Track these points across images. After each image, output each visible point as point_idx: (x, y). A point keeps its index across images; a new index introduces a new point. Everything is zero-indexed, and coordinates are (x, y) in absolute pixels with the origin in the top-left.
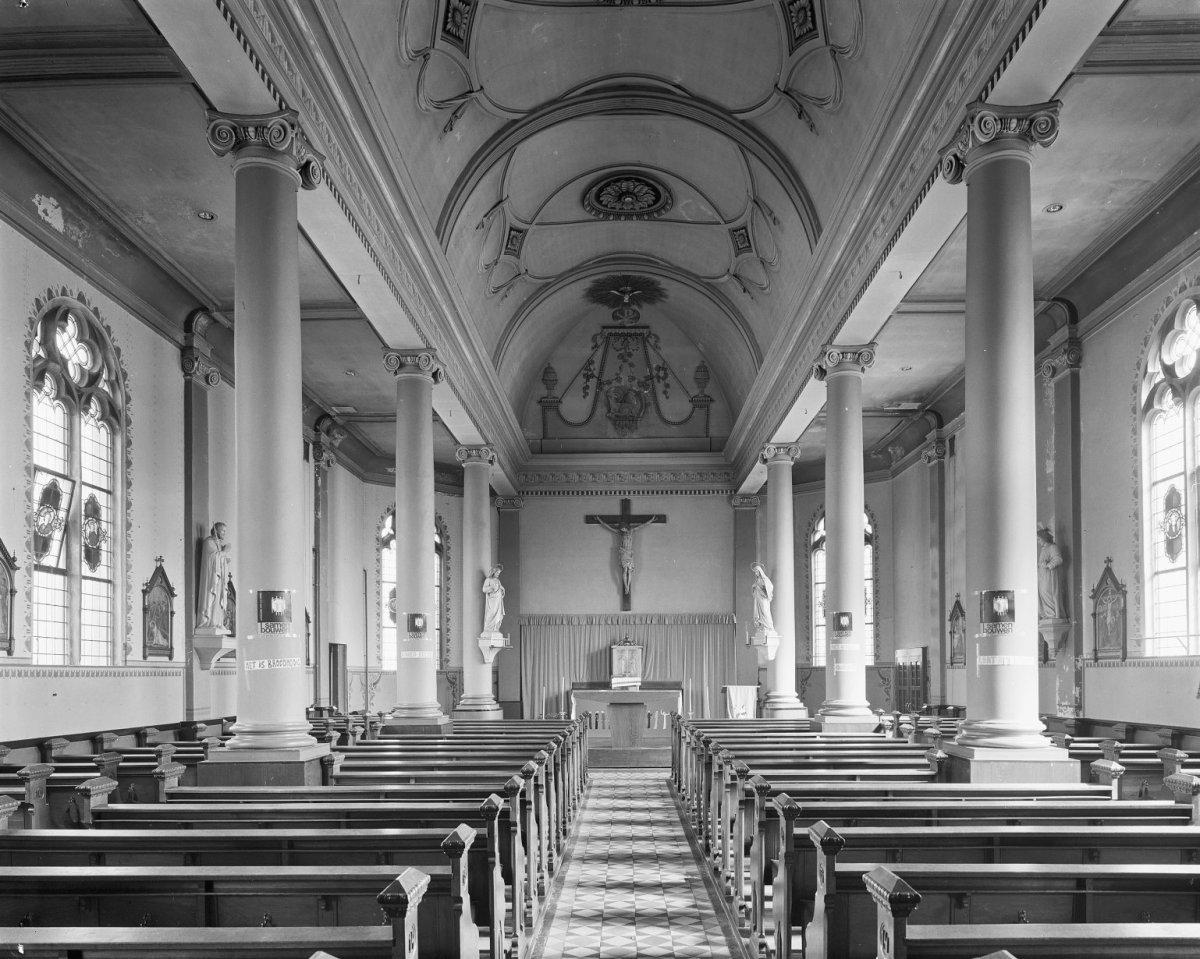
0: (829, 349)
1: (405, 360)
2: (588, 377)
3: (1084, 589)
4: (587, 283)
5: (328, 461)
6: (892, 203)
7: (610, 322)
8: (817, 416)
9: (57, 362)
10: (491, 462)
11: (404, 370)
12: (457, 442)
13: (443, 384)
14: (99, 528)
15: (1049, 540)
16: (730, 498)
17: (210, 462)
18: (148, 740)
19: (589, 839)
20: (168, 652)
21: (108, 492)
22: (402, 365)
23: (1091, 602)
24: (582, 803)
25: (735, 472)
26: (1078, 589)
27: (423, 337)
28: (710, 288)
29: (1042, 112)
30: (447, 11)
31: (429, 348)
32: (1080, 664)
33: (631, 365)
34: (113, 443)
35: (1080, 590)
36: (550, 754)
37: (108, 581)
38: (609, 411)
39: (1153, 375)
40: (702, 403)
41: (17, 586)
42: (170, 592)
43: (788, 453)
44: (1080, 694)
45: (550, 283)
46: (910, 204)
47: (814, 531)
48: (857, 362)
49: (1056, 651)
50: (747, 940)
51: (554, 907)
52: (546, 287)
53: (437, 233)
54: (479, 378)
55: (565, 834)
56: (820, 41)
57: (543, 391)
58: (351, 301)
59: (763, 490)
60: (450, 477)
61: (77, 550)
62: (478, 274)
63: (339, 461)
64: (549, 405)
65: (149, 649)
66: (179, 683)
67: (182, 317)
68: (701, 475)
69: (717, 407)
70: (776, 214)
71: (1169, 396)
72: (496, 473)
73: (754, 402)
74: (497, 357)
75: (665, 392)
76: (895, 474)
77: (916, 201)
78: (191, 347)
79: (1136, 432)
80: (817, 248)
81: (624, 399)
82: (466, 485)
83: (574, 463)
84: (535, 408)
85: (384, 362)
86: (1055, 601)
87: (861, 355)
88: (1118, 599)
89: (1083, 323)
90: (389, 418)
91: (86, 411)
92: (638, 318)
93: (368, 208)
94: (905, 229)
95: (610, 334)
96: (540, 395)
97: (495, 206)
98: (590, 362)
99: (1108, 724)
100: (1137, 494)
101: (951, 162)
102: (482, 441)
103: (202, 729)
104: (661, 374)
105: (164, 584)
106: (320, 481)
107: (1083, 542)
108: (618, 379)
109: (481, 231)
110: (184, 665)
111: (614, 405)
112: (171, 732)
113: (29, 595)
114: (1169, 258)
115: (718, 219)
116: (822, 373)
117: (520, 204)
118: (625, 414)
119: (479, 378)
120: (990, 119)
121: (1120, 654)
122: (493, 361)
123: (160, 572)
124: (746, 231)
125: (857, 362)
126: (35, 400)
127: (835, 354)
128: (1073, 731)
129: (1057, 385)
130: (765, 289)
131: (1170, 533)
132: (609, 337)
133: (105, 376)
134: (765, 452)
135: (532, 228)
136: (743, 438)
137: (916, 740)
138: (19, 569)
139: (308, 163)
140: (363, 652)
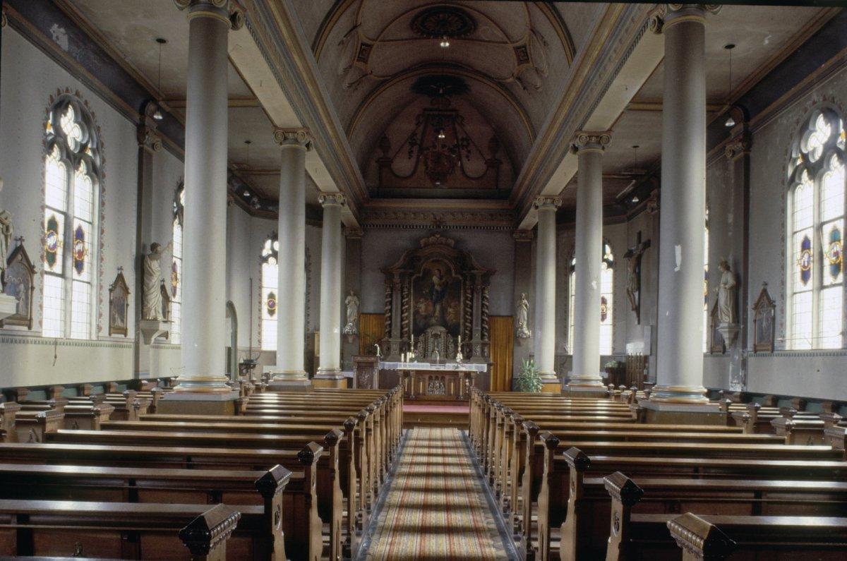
1: (285, 134)
2: (412, 145)
3: (749, 304)
6: (620, 40)
9: (61, 137)
10: (342, 204)
11: (287, 141)
12: (318, 189)
13: (313, 152)
14: (83, 247)
15: (727, 268)
16: (512, 233)
17: (153, 203)
18: (112, 390)
20: (27, 322)
21: (90, 223)
22: (285, 139)
23: (754, 312)
25: (517, 211)
26: (745, 303)
27: (302, 120)
32: (745, 355)
34: (93, 190)
35: (747, 304)
36: (371, 413)
37: (88, 283)
39: (795, 160)
40: (493, 164)
41: (35, 285)
42: (126, 290)
44: (745, 375)
45: (386, 80)
46: (643, 25)
48: (599, 143)
49: (730, 345)
50: (508, 520)
51: (384, 500)
53: (313, 48)
54: (336, 146)
55: (391, 460)
58: (252, 95)
59: (535, 228)
60: (314, 215)
61: (70, 262)
62: (338, 76)
64: (385, 164)
65: (114, 329)
66: (130, 353)
67: (138, 105)
68: (492, 215)
69: (506, 167)
70: (546, 38)
71: (805, 175)
72: (347, 213)
73: (529, 166)
74: (348, 131)
75: (467, 157)
76: (629, 218)
77: (633, 45)
78: (144, 125)
79: (784, 198)
83: (402, 205)
84: (374, 165)
86: (730, 309)
87: (599, 138)
88: (770, 311)
89: (752, 122)
90: (276, 172)
91: (77, 169)
97: (351, 30)
98: (414, 134)
99: (761, 395)
100: (784, 239)
101: (655, 20)
102: (298, 124)
103: (90, 389)
104: (465, 143)
105: (123, 286)
107: (750, 270)
109: (341, 46)
110: (133, 341)
112: (125, 385)
113: (41, 290)
114: (806, 81)
116: (575, 149)
118: (439, 170)
119: (336, 146)
121: (770, 348)
122: (346, 133)
123: (120, 278)
124: (526, 49)
126: (47, 161)
128: (798, 407)
129: (736, 162)
131: (804, 267)
133: (89, 146)
134: (537, 202)
135: (377, 43)
136: (522, 190)
138: (36, 273)
139: (236, 13)
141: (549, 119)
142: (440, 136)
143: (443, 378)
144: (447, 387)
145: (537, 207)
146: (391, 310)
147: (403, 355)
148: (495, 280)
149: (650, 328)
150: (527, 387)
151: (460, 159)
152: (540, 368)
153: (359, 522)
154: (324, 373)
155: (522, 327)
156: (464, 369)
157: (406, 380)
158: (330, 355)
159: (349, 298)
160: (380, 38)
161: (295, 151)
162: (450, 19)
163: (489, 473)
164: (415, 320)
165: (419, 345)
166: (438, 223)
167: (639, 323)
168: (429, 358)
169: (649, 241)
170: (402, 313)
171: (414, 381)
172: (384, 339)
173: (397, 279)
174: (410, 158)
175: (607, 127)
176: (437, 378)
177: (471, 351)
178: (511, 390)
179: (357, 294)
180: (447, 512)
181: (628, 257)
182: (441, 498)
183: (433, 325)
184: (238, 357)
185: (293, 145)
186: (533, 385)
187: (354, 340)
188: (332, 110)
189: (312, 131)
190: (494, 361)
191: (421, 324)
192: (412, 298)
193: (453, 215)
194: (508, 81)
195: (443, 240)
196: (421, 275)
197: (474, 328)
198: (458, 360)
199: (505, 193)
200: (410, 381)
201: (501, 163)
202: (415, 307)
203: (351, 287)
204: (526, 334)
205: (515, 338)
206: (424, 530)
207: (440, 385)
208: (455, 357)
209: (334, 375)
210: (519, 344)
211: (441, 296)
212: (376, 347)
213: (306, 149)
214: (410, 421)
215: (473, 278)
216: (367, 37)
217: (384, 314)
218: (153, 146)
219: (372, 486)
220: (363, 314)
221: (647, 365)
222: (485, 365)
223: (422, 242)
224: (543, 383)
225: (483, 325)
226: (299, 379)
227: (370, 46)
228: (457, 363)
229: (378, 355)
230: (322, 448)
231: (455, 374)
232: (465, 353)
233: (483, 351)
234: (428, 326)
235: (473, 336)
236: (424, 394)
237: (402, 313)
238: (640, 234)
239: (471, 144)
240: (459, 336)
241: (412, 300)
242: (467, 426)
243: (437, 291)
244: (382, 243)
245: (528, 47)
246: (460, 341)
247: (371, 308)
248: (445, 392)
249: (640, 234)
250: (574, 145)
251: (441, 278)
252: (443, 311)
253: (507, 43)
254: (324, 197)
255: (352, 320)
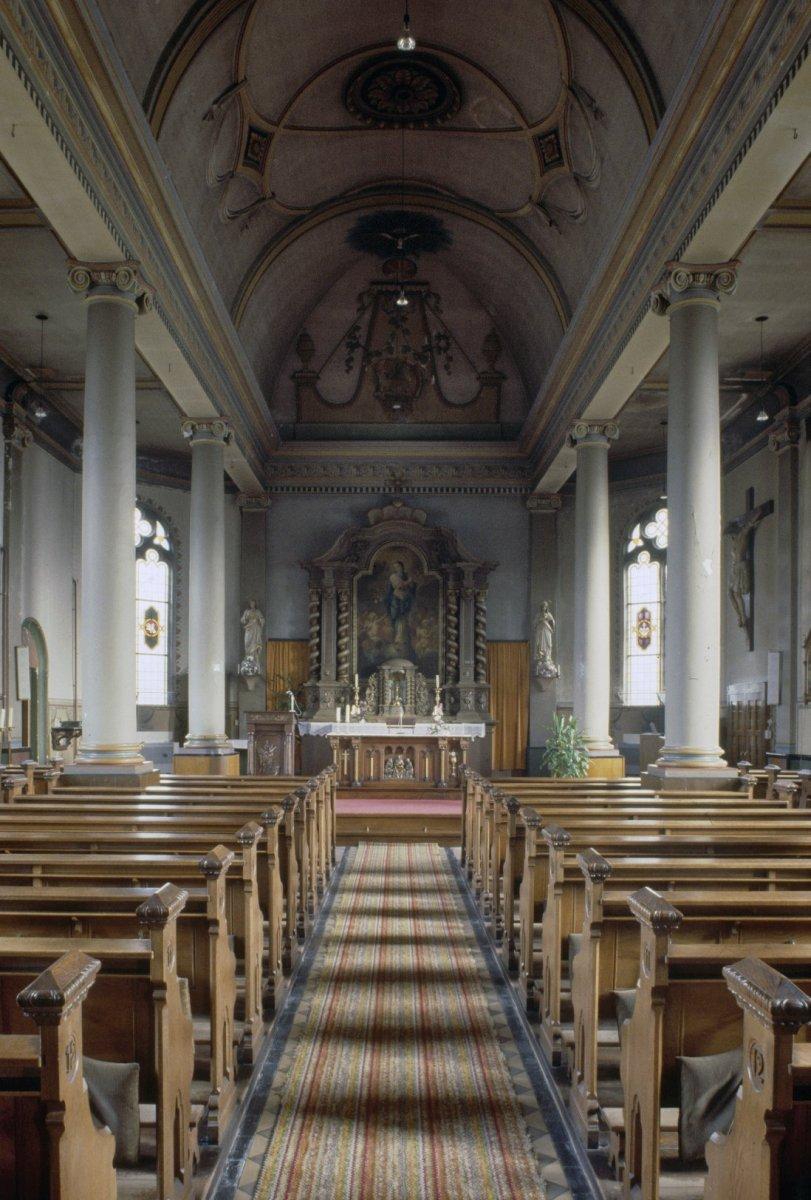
0: (676, 268)
1: (97, 276)
2: (352, 347)
4: (350, 222)
5: (23, 440)
6: (682, 207)
7: (381, 276)
8: (639, 388)
10: (226, 440)
12: (183, 414)
13: (152, 314)
16: (524, 499)
19: (356, 912)
22: (93, 285)
24: (325, 901)
25: (533, 463)
27: (122, 244)
28: (509, 225)
29: (725, 269)
30: (248, 144)
31: (130, 259)
33: (406, 332)
36: (313, 790)
38: (377, 389)
40: (492, 381)
43: (603, 433)
45: (303, 216)
47: (628, 540)
48: (712, 287)
52: (293, 224)
53: (145, 106)
56: (566, 168)
57: (296, 364)
58: (22, 195)
63: (38, 439)
64: (306, 381)
68: (489, 468)
69: (512, 386)
72: (237, 460)
74: (235, 306)
75: (447, 367)
80: (661, 136)
81: (396, 373)
82: (194, 476)
84: (286, 383)
85: (69, 279)
87: (716, 277)
92: (414, 270)
93: (21, 13)
94: (730, 182)
95: (380, 292)
96: (290, 364)
106: (11, 463)
108: (390, 350)
111: (383, 382)
115: (520, 122)
116: (663, 303)
117: (264, 92)
118: (399, 390)
119: (208, 326)
120: (683, 275)
124: (557, 137)
125: (712, 287)
127: (683, 275)
130: (578, 216)
132: (379, 297)
134: (575, 431)
136: (544, 421)
137: (756, 796)
140: (72, 682)
141: (604, 261)
142: (399, 302)
143: (411, 750)
144: (417, 765)
145: (574, 442)
146: (319, 634)
147: (339, 710)
148: (495, 579)
149: (777, 655)
150: (564, 766)
151: (434, 371)
152: (583, 728)
153: (211, 1124)
154: (196, 744)
155: (544, 659)
156: (448, 734)
157: (346, 754)
158: (208, 713)
159: (247, 613)
160: (285, 121)
161: (112, 309)
162: (415, 82)
163: (466, 866)
164: (360, 649)
165: (368, 692)
166: (398, 483)
167: (752, 649)
168: (386, 715)
169: (771, 503)
170: (339, 637)
171: (360, 758)
172: (309, 684)
173: (328, 579)
174: (347, 371)
175: (731, 253)
176: (400, 750)
177: (457, 701)
178: (525, 773)
179: (262, 607)
180: (432, 1132)
181: (731, 532)
182: (406, 902)
183: (391, 658)
184: (50, 718)
185: (108, 297)
186: (575, 761)
187: (256, 686)
188: (197, 255)
189: (146, 267)
190: (497, 718)
191: (371, 656)
192: (355, 611)
193: (424, 468)
194: (521, 213)
195: (408, 511)
196: (370, 572)
197: (463, 662)
198: (437, 718)
199: (511, 428)
200: (352, 756)
201: (504, 378)
202: (360, 627)
203: (247, 595)
204: (551, 671)
205: (532, 678)
206: (384, 941)
207: (406, 763)
208: (429, 712)
209: (215, 748)
210: (540, 689)
211: (403, 612)
212: (288, 697)
213: (225, 443)
214: (350, 833)
215: (460, 576)
216: (283, 206)
217: (307, 641)
218: (23, 442)
219: (324, 869)
220: (270, 640)
221: (770, 722)
222: (483, 726)
223: (372, 515)
224: (591, 757)
225: (478, 657)
226: (128, 761)
227: (267, 137)
228: (434, 722)
229: (293, 710)
230: (232, 854)
231: (432, 742)
232: (448, 704)
233: (478, 701)
234: (383, 659)
235: (461, 675)
236: (378, 779)
237: (339, 637)
238: (751, 493)
239: (453, 345)
240: (437, 677)
241: (355, 616)
242: (461, 839)
243: (398, 600)
244: (300, 518)
245: (561, 131)
246: (438, 685)
247: (285, 630)
248: (414, 775)
249: (751, 493)
250: (660, 296)
251: (404, 577)
252: (410, 633)
253: (521, 129)
254: (193, 427)
255: (252, 650)
